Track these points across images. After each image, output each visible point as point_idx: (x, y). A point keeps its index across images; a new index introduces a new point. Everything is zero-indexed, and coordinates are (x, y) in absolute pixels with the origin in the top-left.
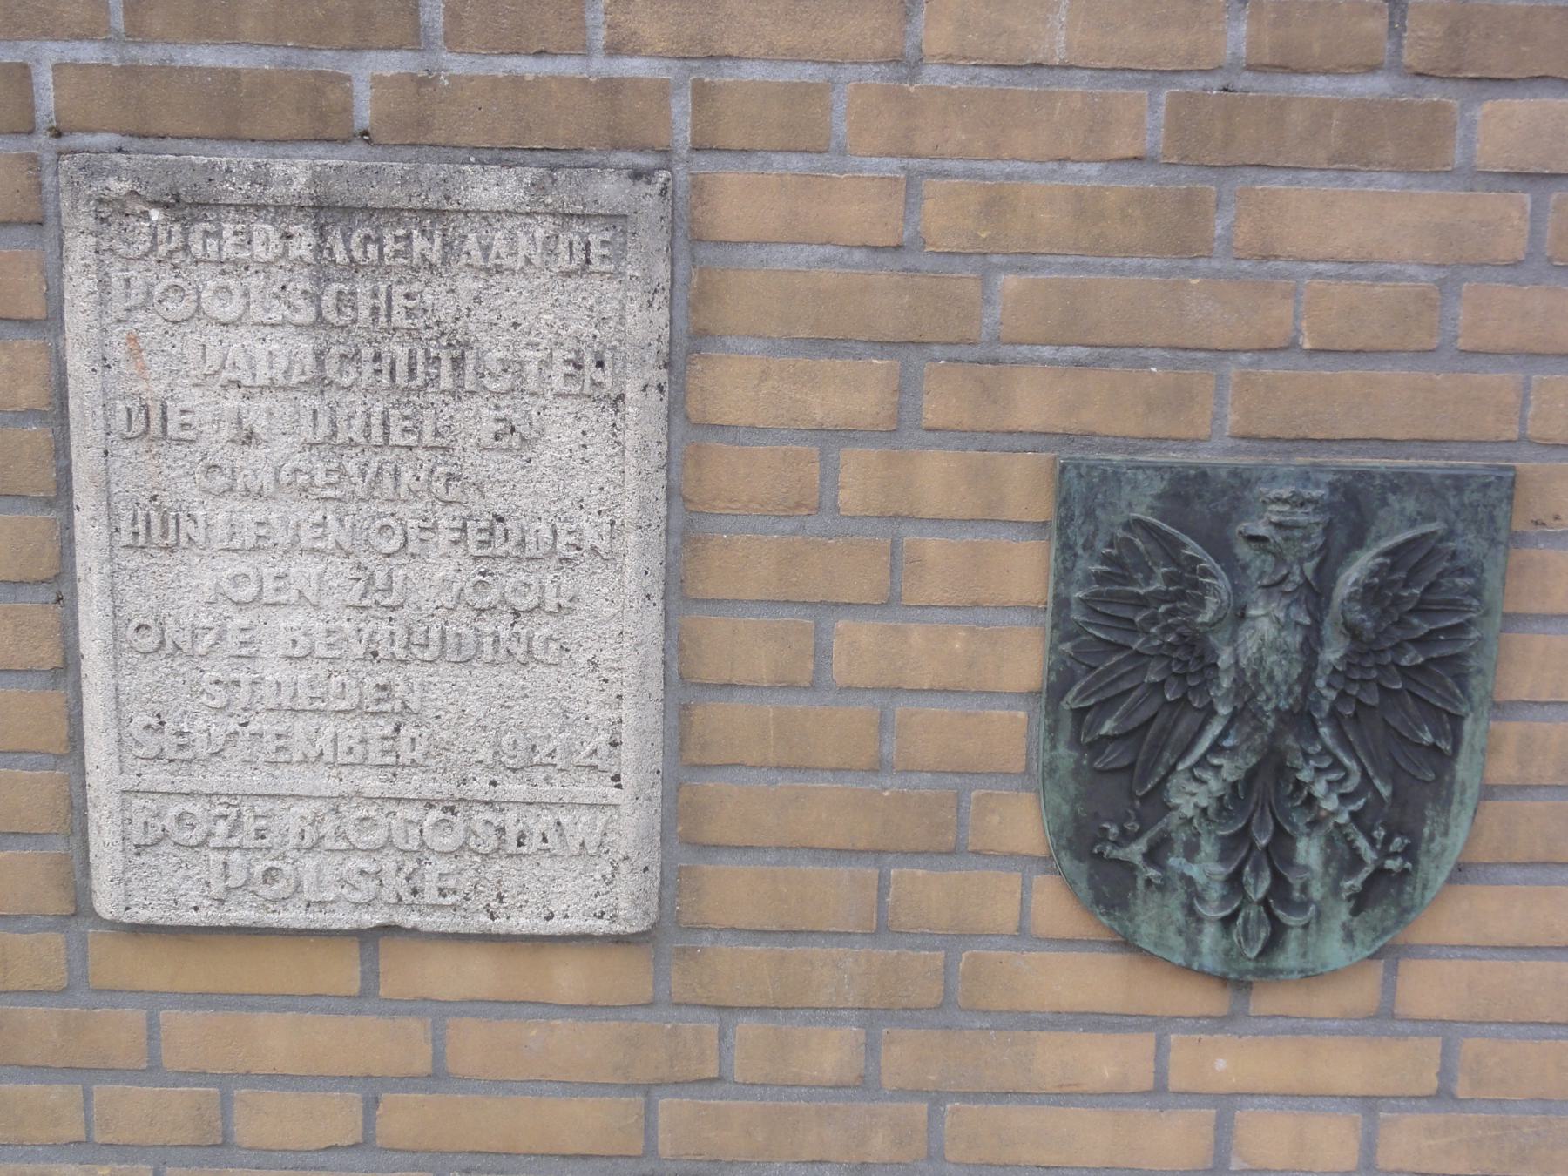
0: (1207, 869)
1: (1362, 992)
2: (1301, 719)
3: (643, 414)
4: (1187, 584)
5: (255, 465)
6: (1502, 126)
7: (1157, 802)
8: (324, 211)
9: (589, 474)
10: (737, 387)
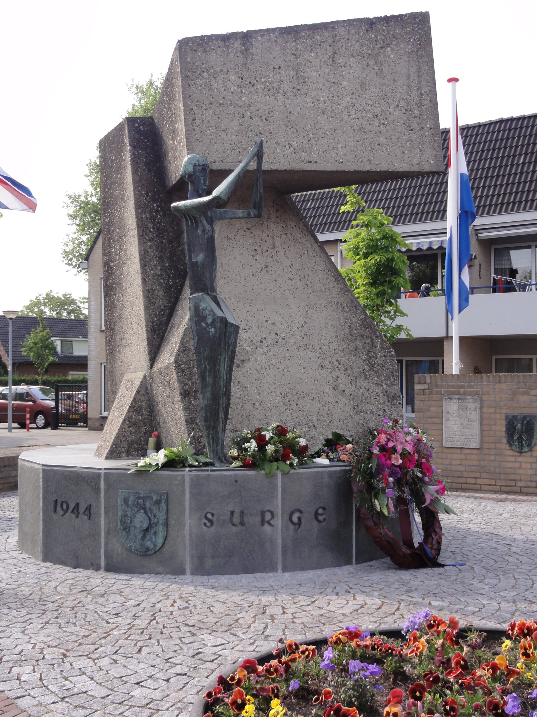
0: (516, 443)
1: (529, 454)
2: (522, 432)
3: (478, 412)
4: (514, 423)
5: (454, 415)
6: (533, 392)
7: (513, 439)
8: (459, 399)
9: (475, 416)
10: (485, 410)
